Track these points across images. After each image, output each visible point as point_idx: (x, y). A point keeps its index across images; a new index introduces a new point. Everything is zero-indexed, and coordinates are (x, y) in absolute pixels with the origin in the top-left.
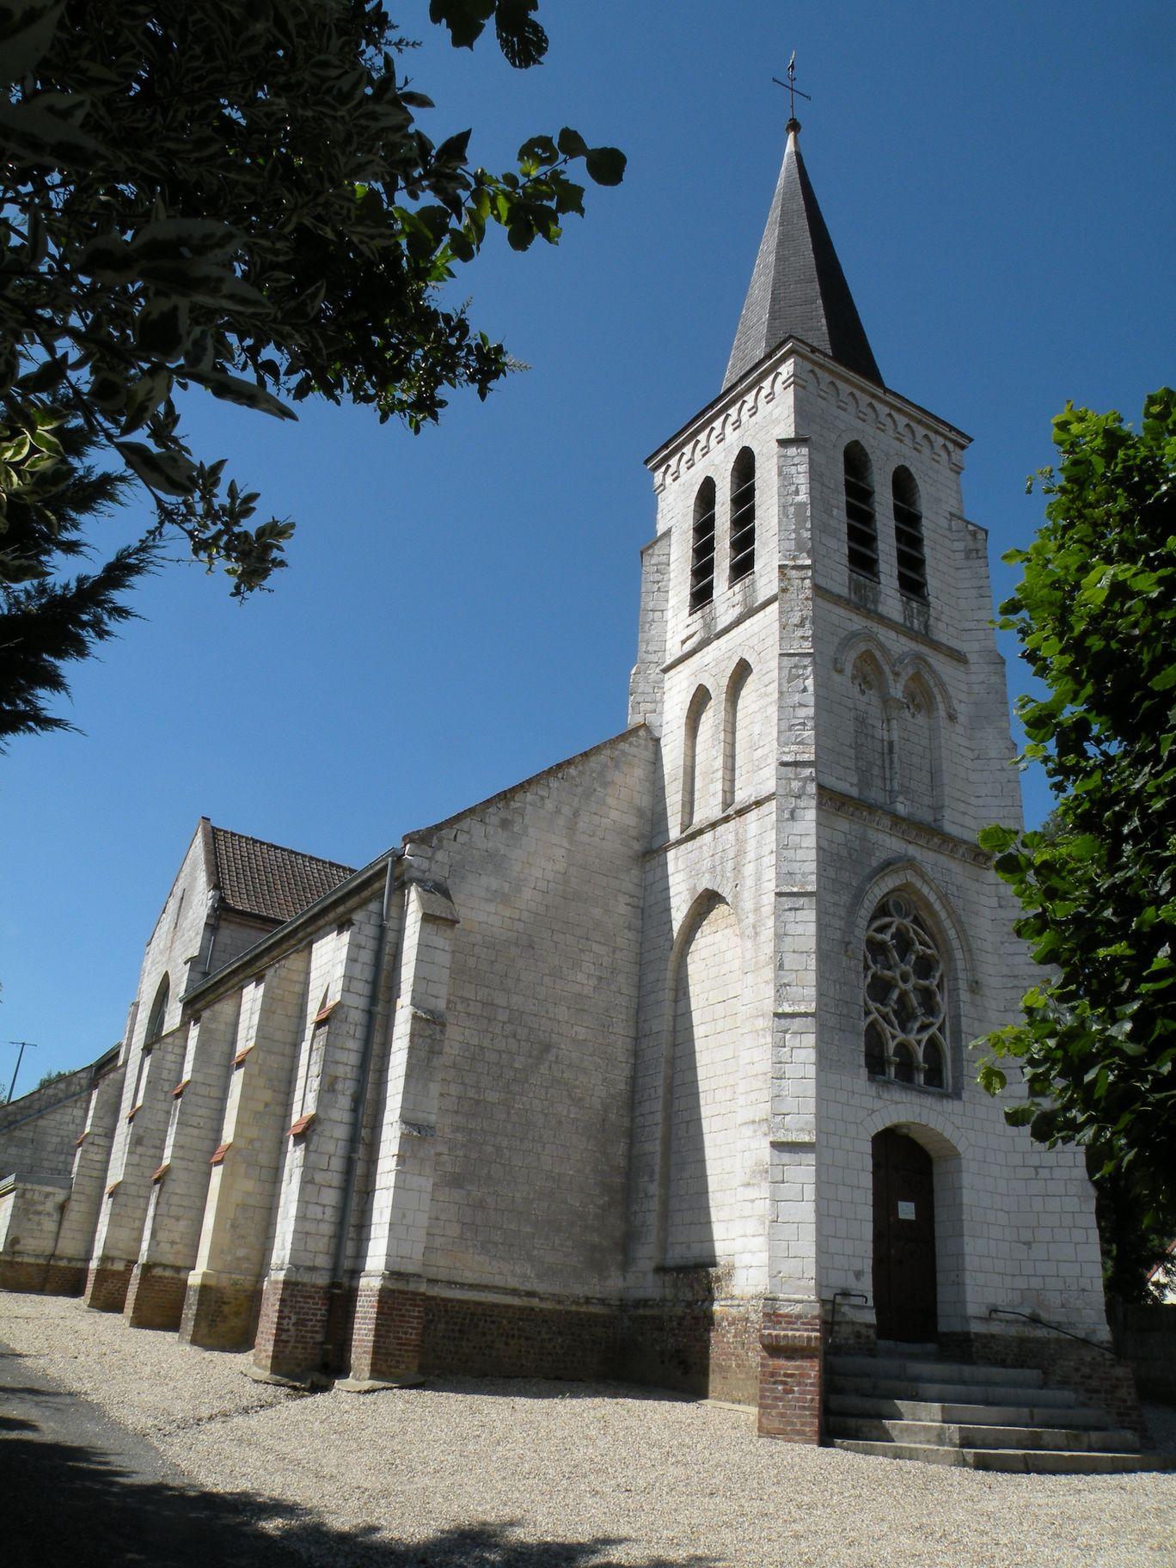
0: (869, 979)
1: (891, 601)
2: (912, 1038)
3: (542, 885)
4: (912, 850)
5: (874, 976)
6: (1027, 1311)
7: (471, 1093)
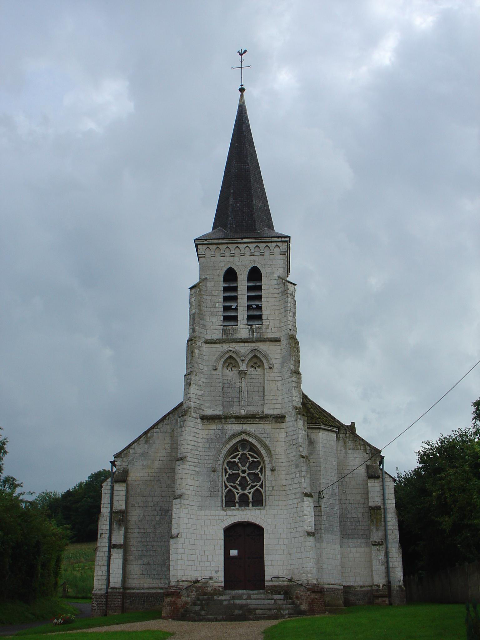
0: (227, 476)
1: (243, 329)
2: (246, 492)
3: (162, 459)
4: (245, 427)
5: (230, 475)
6: (289, 577)
7: (142, 531)
